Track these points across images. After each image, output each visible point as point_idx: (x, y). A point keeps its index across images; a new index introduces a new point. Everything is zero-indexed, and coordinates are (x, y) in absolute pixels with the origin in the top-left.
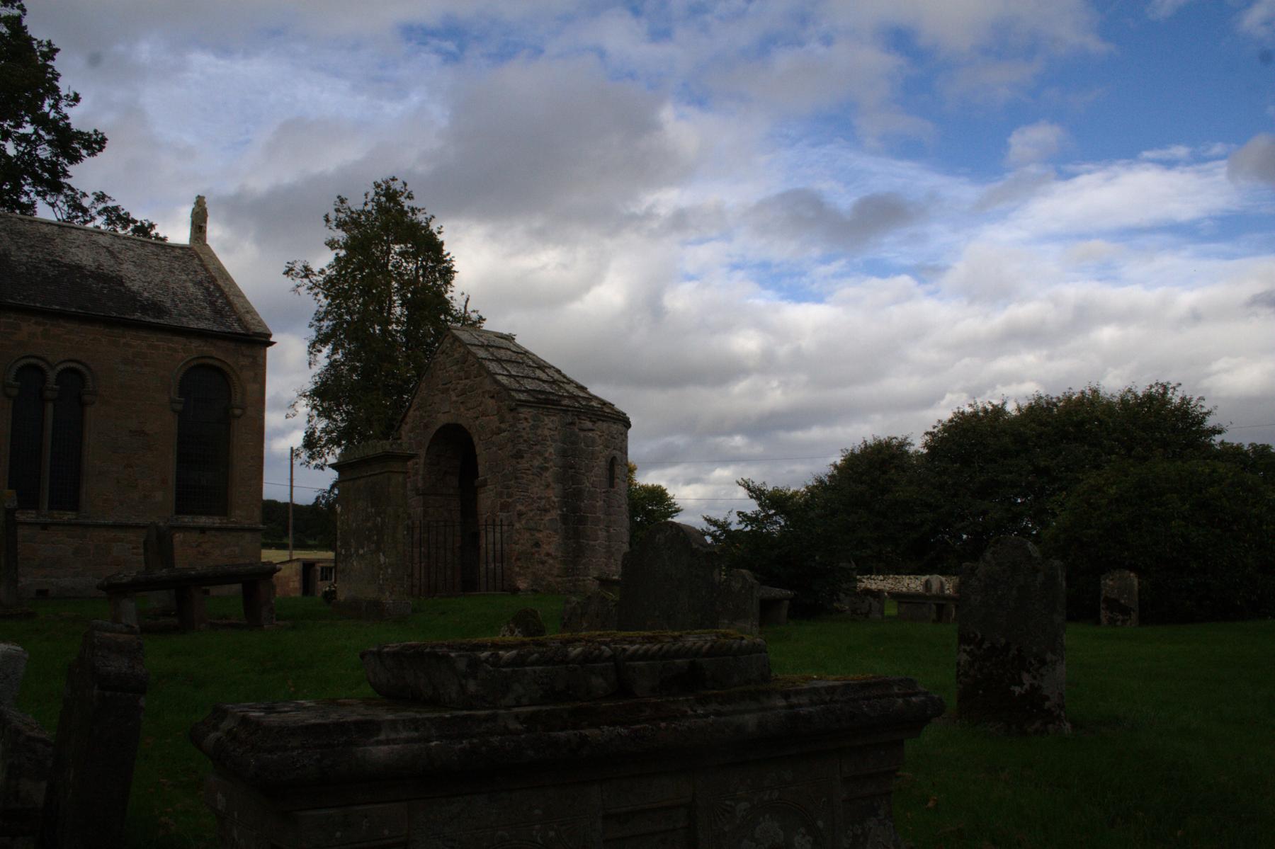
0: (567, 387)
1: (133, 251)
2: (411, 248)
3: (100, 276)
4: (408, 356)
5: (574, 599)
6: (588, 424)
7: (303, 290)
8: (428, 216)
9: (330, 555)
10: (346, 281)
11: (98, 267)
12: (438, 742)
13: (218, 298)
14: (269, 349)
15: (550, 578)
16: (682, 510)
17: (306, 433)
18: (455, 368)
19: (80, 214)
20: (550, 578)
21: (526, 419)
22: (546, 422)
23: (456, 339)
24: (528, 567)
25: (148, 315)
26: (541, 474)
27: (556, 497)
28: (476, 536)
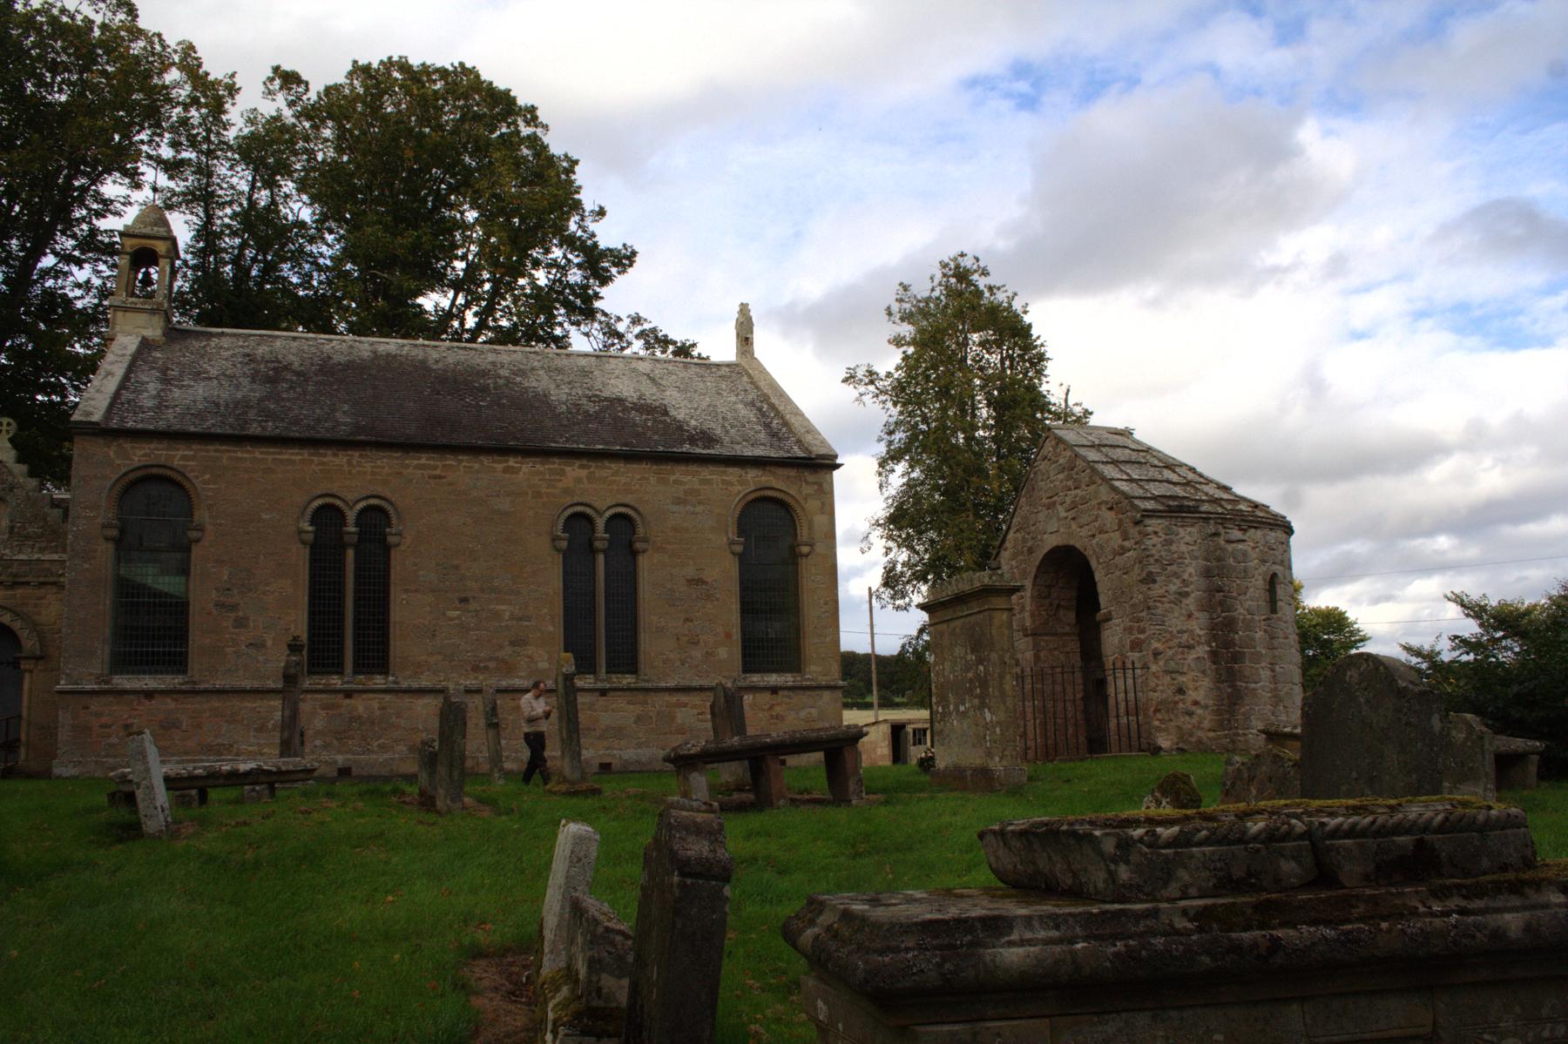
0: (1205, 488)
1: (676, 374)
2: (992, 335)
3: (643, 408)
4: (1000, 468)
5: (1237, 758)
6: (1237, 534)
7: (867, 399)
8: (1010, 294)
9: (924, 714)
10: (917, 384)
11: (640, 398)
12: (1086, 944)
13: (773, 418)
14: (836, 473)
15: (1200, 733)
16: (1369, 638)
17: (885, 568)
18: (1061, 476)
19: (616, 341)
20: (1200, 733)
21: (1156, 533)
22: (1181, 536)
23: (1060, 440)
24: (1171, 720)
25: (697, 445)
26: (1181, 602)
27: (1201, 629)
28: (1101, 684)
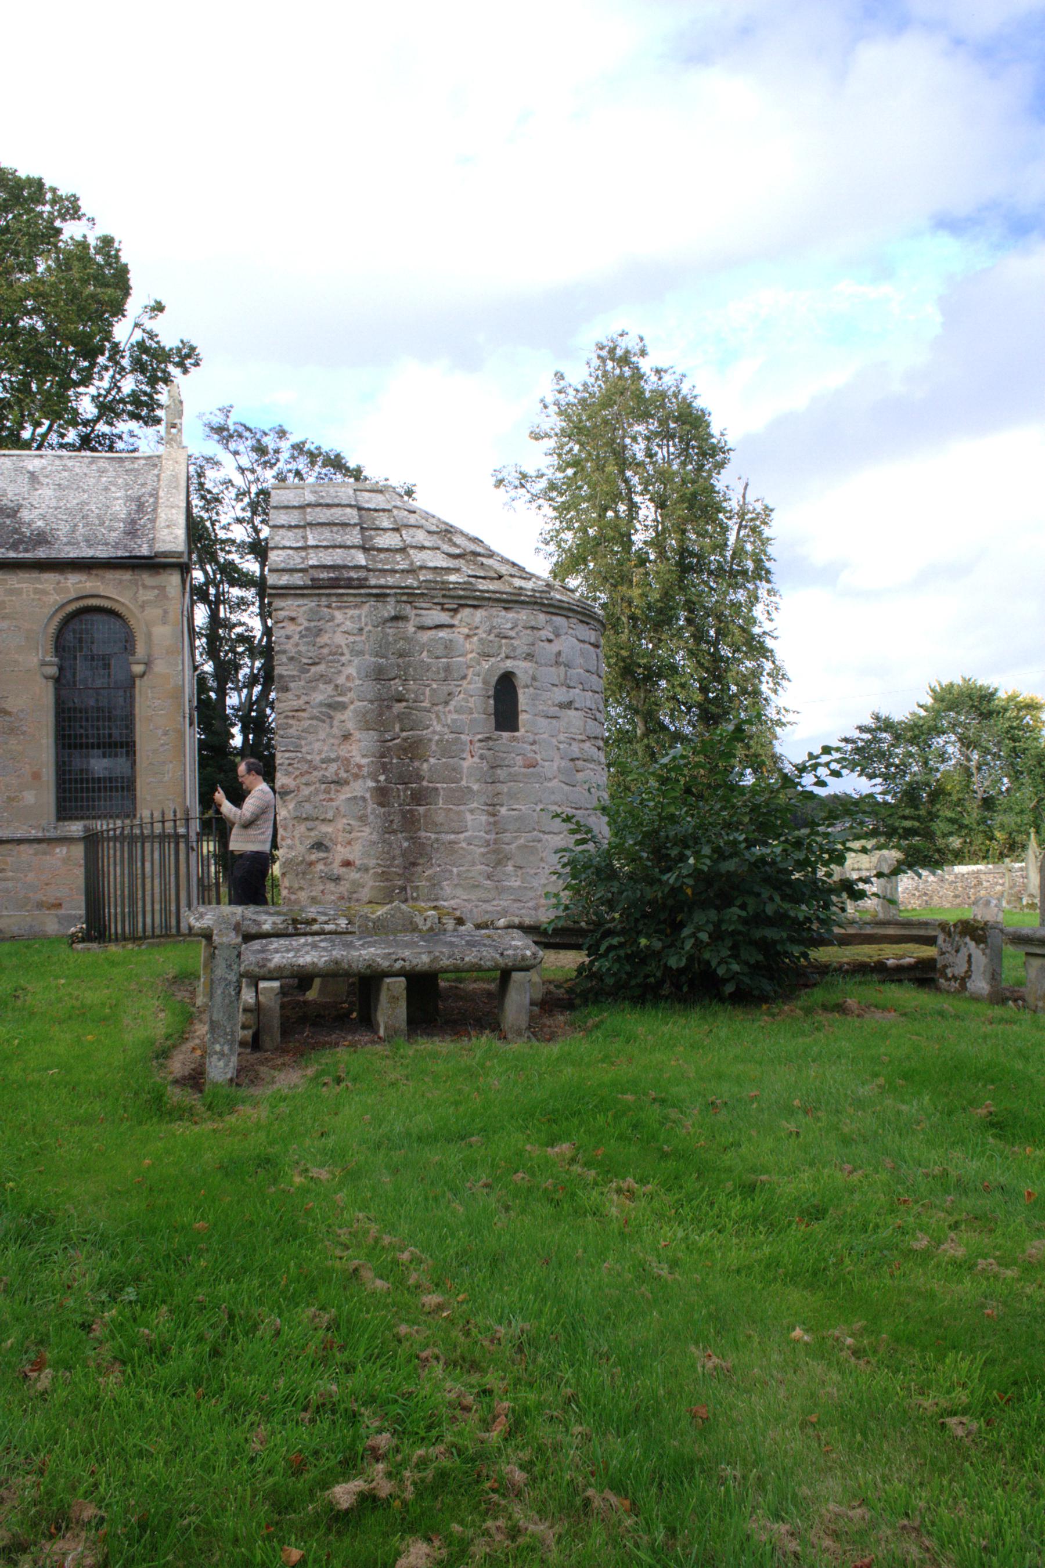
7: (519, 504)
21: (292, 619)
22: (337, 621)
26: (331, 718)
27: (364, 756)
